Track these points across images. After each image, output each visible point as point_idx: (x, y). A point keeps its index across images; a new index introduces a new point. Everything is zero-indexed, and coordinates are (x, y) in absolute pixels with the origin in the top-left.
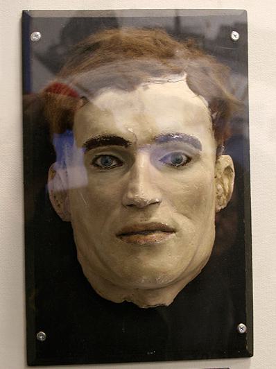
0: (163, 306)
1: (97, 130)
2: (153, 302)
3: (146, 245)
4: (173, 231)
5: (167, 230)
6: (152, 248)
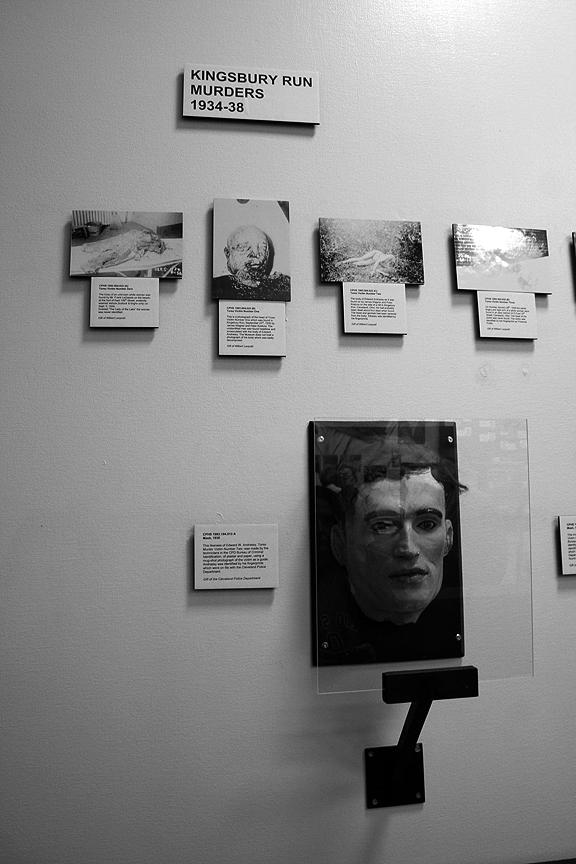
0: (412, 623)
1: (377, 505)
2: (407, 621)
3: (410, 584)
4: (427, 573)
5: (422, 572)
6: (415, 586)
